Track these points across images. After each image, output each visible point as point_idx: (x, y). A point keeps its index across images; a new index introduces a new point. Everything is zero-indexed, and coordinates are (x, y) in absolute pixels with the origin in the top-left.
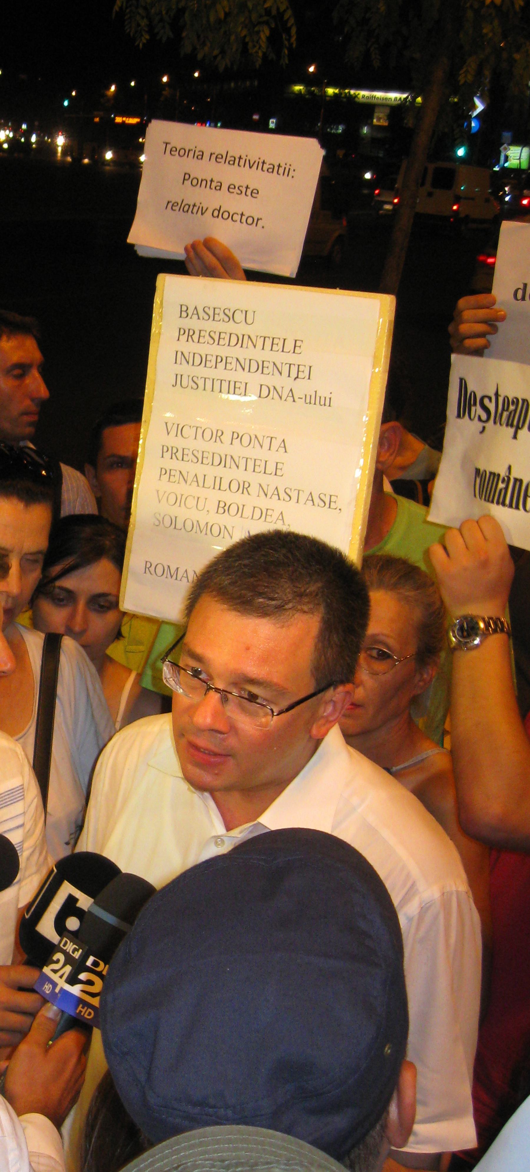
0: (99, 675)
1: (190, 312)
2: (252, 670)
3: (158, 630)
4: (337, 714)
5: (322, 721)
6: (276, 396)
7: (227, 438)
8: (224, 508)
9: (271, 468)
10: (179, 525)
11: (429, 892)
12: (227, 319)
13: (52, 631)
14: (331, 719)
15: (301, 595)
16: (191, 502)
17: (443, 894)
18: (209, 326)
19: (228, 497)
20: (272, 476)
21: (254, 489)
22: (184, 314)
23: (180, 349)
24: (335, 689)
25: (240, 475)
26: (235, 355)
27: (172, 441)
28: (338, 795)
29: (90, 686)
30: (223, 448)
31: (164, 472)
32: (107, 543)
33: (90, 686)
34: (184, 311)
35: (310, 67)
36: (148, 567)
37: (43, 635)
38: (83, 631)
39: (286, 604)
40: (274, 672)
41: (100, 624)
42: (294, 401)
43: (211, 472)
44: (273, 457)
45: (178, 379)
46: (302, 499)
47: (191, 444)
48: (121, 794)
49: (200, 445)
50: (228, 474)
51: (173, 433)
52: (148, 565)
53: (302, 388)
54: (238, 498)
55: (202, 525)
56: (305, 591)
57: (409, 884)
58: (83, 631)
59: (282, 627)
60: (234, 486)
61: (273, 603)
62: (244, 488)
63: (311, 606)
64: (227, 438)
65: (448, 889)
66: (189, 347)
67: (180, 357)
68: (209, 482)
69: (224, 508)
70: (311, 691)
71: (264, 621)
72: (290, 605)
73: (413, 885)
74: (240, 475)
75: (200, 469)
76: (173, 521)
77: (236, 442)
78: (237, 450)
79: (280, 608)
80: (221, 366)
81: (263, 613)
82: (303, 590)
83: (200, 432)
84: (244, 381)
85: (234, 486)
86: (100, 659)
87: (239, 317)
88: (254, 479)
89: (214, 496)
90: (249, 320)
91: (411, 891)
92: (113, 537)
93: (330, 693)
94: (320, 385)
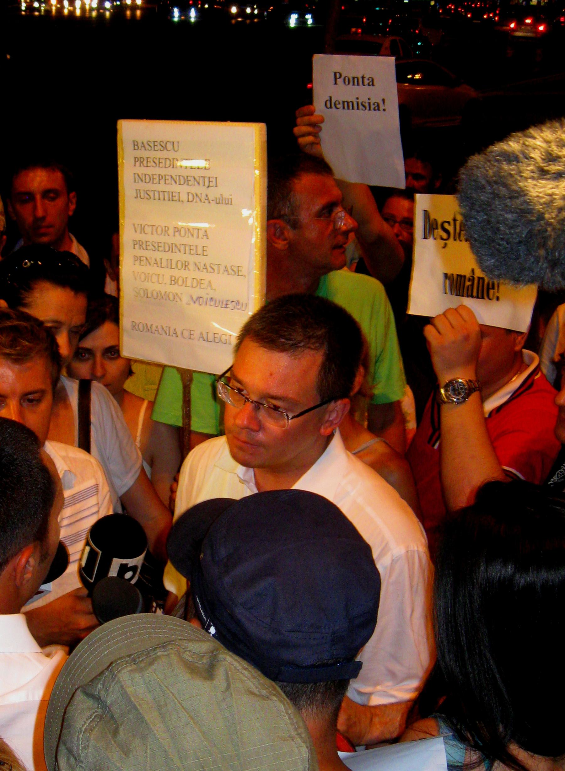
0: (120, 407)
1: (140, 145)
2: (274, 391)
3: (163, 372)
4: (338, 420)
5: (327, 425)
6: (198, 200)
7: (171, 232)
8: (174, 281)
9: (200, 251)
10: (149, 295)
11: (397, 550)
12: (162, 149)
13: (83, 378)
14: (335, 422)
15: (310, 337)
16: (155, 279)
17: (407, 552)
18: (152, 154)
19: (177, 273)
20: (202, 256)
21: (191, 266)
22: (136, 148)
23: (137, 172)
24: (335, 402)
25: (184, 257)
26: (158, 173)
27: (140, 237)
28: (342, 479)
29: (115, 415)
30: (171, 240)
31: (137, 258)
32: (108, 310)
33: (115, 415)
34: (136, 145)
35: (540, 26)
36: (134, 326)
37: (78, 381)
38: (104, 376)
39: (299, 343)
40: (291, 391)
41: (113, 368)
42: (209, 203)
43: (165, 256)
44: (200, 242)
45: (138, 191)
46: (221, 271)
47: (150, 238)
48: (195, 487)
49: (155, 238)
50: (176, 257)
51: (138, 230)
52: (134, 324)
53: (213, 193)
54: (183, 273)
55: (163, 293)
56: (313, 334)
57: (384, 544)
58: (104, 376)
59: (295, 359)
60: (179, 265)
61: (291, 342)
62: (186, 266)
63: (317, 345)
64: (171, 232)
65: (411, 548)
66: (142, 170)
67: (137, 178)
68: (164, 264)
69: (174, 281)
70: (318, 403)
71: (283, 354)
72: (302, 344)
73: (386, 545)
74: (184, 257)
75: (158, 255)
76: (146, 292)
77: (177, 234)
78: (177, 240)
79: (295, 346)
80: (162, 182)
81: (283, 349)
82: (311, 333)
83: (155, 228)
84: (177, 191)
85: (179, 265)
86: (119, 394)
87: (169, 146)
88: (192, 259)
89: (168, 273)
90: (176, 148)
91: (385, 549)
92: (111, 305)
93: (332, 404)
94: (223, 190)
